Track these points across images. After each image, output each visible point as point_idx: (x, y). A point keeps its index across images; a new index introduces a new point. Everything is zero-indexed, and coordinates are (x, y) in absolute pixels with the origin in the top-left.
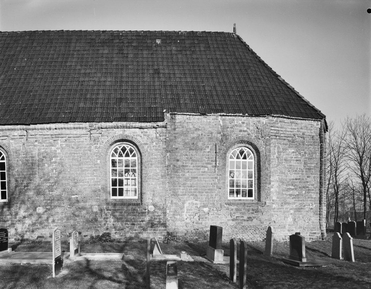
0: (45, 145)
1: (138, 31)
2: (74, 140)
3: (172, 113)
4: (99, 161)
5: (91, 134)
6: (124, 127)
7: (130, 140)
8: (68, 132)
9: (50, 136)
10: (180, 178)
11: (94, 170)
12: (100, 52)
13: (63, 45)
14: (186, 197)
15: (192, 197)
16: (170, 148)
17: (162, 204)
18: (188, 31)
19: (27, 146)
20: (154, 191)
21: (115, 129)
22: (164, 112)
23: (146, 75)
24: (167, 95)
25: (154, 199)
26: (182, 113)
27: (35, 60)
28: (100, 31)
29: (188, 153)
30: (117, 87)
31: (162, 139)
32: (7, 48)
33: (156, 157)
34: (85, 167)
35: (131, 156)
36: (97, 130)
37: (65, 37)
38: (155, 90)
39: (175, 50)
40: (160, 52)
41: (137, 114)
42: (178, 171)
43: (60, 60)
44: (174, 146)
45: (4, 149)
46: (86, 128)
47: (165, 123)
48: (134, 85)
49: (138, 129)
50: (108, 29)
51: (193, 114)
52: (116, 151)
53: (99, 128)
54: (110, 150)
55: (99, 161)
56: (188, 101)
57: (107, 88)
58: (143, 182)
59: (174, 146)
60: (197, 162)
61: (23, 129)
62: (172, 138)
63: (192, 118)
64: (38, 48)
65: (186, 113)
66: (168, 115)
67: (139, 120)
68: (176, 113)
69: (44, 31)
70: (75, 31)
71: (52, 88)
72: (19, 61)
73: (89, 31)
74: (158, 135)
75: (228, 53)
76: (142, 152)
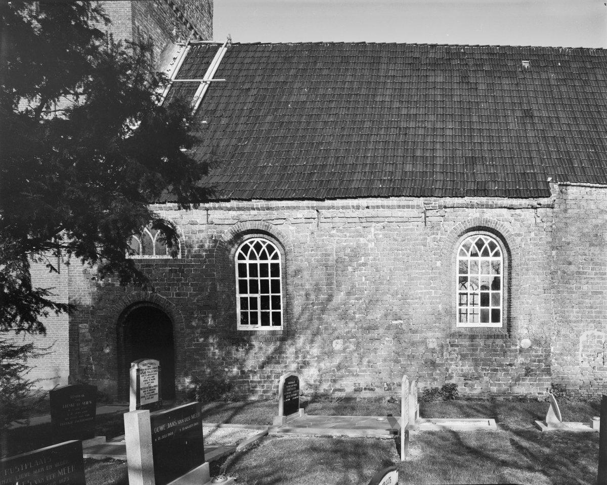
0: (348, 235)
1: (490, 45)
2: (398, 227)
3: (562, 183)
4: (439, 264)
5: (428, 217)
6: (483, 205)
7: (492, 229)
8: (387, 212)
9: (357, 220)
10: (573, 292)
11: (432, 278)
12: (431, 79)
13: (367, 66)
14: (582, 324)
15: (592, 325)
16: (557, 244)
17: (544, 337)
18: (574, 47)
19: (318, 236)
20: (530, 315)
21: (466, 209)
22: (549, 182)
23: (510, 120)
24: (549, 153)
25: (530, 328)
26: (578, 184)
27: (321, 91)
28: (426, 44)
29: (587, 252)
30: (465, 140)
31: (545, 227)
32: (273, 70)
33: (534, 257)
34: (415, 272)
35: (491, 254)
36: (437, 210)
37: (369, 54)
38: (528, 144)
39: (555, 78)
40: (529, 82)
41: (504, 183)
42: (570, 281)
43: (363, 92)
44: (563, 240)
45: (278, 240)
46: (418, 207)
47: (553, 199)
48: (493, 136)
49: (506, 209)
50: (440, 42)
51: (598, 185)
52: (467, 247)
53: (440, 207)
54: (458, 244)
55: (439, 264)
56: (585, 164)
57: (449, 139)
58: (512, 299)
59: (563, 240)
60: (603, 267)
61: (313, 208)
62: (562, 225)
63: (595, 192)
64: (325, 72)
65: (585, 184)
66: (556, 186)
67: (508, 194)
68: (568, 183)
69: (333, 44)
70: (385, 43)
71: (355, 139)
72: (295, 92)
73: (409, 44)
74: (538, 220)
75: (246, 86)
76: (511, 248)
